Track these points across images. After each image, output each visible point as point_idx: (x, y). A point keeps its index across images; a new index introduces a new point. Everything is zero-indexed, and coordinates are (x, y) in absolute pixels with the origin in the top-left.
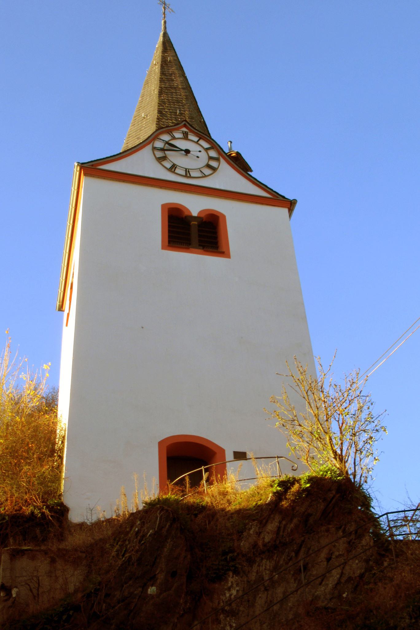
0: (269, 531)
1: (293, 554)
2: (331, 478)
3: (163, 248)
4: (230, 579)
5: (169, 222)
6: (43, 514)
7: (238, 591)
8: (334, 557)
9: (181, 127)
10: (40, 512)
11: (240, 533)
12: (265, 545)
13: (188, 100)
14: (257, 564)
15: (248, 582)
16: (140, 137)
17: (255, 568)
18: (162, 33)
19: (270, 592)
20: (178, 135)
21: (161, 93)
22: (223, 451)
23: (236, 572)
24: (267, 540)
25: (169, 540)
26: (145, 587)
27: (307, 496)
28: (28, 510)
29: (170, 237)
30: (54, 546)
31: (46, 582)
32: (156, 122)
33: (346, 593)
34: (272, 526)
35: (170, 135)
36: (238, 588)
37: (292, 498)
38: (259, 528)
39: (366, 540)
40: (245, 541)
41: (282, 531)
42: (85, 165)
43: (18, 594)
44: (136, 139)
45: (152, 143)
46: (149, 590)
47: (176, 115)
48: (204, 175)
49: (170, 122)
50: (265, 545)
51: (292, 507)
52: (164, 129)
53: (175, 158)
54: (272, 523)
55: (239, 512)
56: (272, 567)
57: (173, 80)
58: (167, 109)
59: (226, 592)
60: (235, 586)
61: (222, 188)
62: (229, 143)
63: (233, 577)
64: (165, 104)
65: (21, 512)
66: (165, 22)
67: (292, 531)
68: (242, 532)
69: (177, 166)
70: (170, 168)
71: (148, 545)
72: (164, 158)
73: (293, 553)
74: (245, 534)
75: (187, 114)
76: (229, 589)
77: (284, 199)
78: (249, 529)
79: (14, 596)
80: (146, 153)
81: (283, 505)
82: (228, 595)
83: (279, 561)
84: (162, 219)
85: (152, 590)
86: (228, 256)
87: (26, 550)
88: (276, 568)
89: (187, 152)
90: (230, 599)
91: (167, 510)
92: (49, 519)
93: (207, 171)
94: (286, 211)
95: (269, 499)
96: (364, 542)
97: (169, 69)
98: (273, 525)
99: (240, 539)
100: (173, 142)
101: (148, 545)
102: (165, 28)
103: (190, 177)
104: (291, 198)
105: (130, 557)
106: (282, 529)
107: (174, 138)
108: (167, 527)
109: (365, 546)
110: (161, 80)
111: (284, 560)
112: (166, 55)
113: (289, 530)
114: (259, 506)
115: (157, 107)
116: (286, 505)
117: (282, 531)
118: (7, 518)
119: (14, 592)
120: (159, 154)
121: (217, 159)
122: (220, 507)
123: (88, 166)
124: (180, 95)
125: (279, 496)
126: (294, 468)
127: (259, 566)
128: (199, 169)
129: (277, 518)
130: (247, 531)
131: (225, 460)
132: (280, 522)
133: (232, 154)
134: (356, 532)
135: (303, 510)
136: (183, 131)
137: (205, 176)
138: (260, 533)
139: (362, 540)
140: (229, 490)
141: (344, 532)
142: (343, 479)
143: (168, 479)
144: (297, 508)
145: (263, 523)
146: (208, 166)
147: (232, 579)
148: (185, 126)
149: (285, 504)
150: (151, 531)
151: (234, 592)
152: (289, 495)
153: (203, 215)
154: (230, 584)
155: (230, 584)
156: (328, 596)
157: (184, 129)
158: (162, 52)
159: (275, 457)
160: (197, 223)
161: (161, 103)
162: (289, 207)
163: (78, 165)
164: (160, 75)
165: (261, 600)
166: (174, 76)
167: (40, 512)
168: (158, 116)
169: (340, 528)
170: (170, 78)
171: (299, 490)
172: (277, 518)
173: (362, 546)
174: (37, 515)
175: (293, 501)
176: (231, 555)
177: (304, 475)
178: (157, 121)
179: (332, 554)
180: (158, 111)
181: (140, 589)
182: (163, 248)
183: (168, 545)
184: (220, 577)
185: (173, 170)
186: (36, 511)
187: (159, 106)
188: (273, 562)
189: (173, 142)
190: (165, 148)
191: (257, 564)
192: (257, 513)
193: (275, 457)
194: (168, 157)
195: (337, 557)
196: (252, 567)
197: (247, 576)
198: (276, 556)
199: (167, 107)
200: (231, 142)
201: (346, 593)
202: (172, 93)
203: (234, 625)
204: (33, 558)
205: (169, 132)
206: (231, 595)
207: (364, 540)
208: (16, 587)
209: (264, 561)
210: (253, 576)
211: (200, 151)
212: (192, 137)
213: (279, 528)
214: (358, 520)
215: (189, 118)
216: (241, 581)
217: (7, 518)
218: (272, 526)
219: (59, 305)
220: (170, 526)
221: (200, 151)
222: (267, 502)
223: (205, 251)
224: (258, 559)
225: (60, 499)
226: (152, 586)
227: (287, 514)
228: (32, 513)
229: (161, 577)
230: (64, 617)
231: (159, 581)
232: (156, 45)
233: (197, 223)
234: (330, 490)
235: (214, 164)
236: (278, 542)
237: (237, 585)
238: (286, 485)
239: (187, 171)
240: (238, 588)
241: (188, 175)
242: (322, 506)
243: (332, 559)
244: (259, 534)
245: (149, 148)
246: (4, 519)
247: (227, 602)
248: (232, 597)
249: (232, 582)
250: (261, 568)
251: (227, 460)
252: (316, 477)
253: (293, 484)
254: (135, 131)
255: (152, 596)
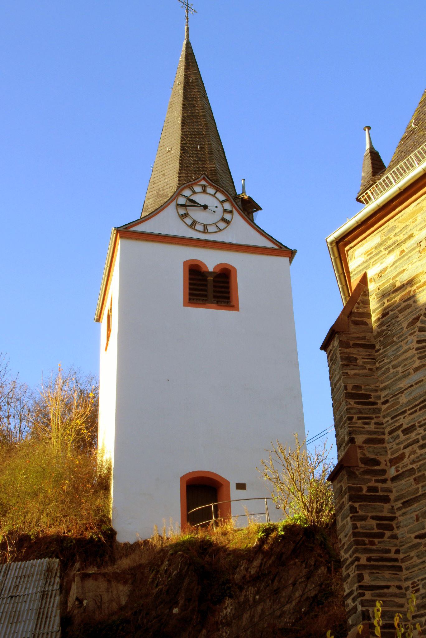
0: (254, 566)
1: (270, 582)
2: (300, 525)
3: (185, 305)
4: (227, 602)
5: (190, 274)
6: (99, 538)
7: (231, 609)
8: (298, 583)
9: (200, 181)
10: (97, 537)
11: (235, 568)
12: (251, 576)
13: (207, 130)
14: (245, 590)
15: (239, 603)
16: (165, 174)
17: (243, 593)
18: (185, 42)
19: (253, 610)
20: (198, 189)
21: (183, 124)
22: (228, 483)
23: (231, 597)
24: (252, 573)
25: (187, 578)
26: (171, 609)
27: (281, 540)
28: (88, 534)
29: (190, 294)
30: (110, 569)
31: (105, 598)
32: (178, 178)
33: (304, 608)
34: (256, 563)
35: (191, 189)
36: (232, 607)
37: (272, 543)
38: (248, 565)
39: (321, 569)
40: (238, 574)
41: (263, 566)
42: (120, 229)
43: (88, 604)
44: (162, 176)
45: (175, 201)
46: (174, 610)
47: (197, 150)
48: (219, 230)
49: (192, 160)
50: (251, 576)
51: (271, 549)
52: (186, 185)
53: (196, 214)
54: (256, 560)
55: (235, 551)
56: (255, 592)
57: (194, 106)
58: (189, 144)
59: (224, 610)
60: (230, 606)
61: (235, 242)
62: (243, 180)
63: (229, 600)
64: (187, 138)
65: (84, 536)
66: (188, 29)
67: (270, 565)
68: (236, 569)
69: (197, 222)
70: (191, 225)
71: (173, 582)
72: (186, 215)
73: (270, 581)
74: (238, 569)
75: (206, 148)
76: (226, 608)
77: (289, 250)
78: (241, 566)
79: (85, 605)
80: (171, 211)
81: (264, 548)
82: (225, 612)
83: (260, 587)
84: (181, 518)
85: (176, 610)
86: (238, 310)
87: (92, 574)
88: (257, 593)
89: (205, 207)
90: (226, 615)
91: (186, 557)
92: (103, 542)
93: (222, 225)
94: (287, 259)
95: (255, 543)
96: (320, 572)
97: (191, 92)
98: (257, 562)
99: (234, 574)
100: (193, 198)
101: (173, 582)
102: (188, 36)
103: (208, 232)
104: (292, 248)
105: (162, 589)
106: (263, 564)
107: (194, 193)
108: (186, 569)
109: (320, 574)
110: (184, 107)
111: (264, 586)
112: (189, 73)
113: (268, 565)
114: (248, 548)
115: (179, 142)
116: (266, 548)
117: (263, 566)
118: (74, 541)
119: (85, 602)
120: (182, 211)
121: (230, 212)
122: (222, 544)
123: (122, 230)
124: (201, 125)
125: (262, 541)
126: (277, 507)
127: (246, 591)
128: (215, 223)
129: (261, 556)
130: (239, 567)
131: (230, 499)
132: (262, 560)
133: (244, 197)
134: (315, 564)
135: (278, 550)
136: (202, 185)
137: (220, 230)
138: (248, 568)
139: (318, 570)
140: (229, 530)
141: (306, 564)
142: (308, 526)
143: (188, 522)
144: (275, 549)
145: (250, 561)
146: (223, 220)
147: (228, 601)
148: (204, 179)
149: (266, 547)
150: (175, 572)
151: (229, 610)
152: (270, 541)
153: (217, 271)
154: (226, 605)
155: (226, 605)
156: (292, 611)
157: (203, 182)
158: (185, 69)
159: (264, 498)
160: (212, 278)
161: (184, 137)
162: (290, 256)
163: (115, 230)
164: (183, 101)
165: (246, 616)
166: (196, 101)
167: (97, 537)
168: (181, 153)
169: (304, 561)
170: (192, 104)
171: (276, 536)
172: (261, 556)
173: (318, 575)
174: (95, 539)
175: (272, 545)
176: (228, 585)
177: (282, 523)
178: (181, 134)
179: (296, 581)
180: (181, 147)
181: (168, 610)
182: (185, 305)
183: (186, 581)
184: (220, 601)
185: (193, 227)
186: (94, 537)
187: (182, 141)
188: (256, 589)
189: (194, 198)
190: (187, 204)
191: (245, 590)
192: (246, 554)
193: (264, 498)
194: (189, 214)
195: (300, 583)
196: (241, 592)
197: (238, 599)
198: (258, 583)
199: (189, 141)
200: (244, 180)
201: (304, 608)
202: (193, 122)
203: (228, 632)
204: (96, 579)
205: (190, 187)
206: (227, 612)
207: (320, 570)
208: (86, 599)
209: (250, 588)
210: (242, 599)
211: (216, 207)
212: (211, 191)
213: (261, 564)
214: (316, 555)
215: (208, 153)
216: (234, 602)
217: (74, 541)
218: (256, 563)
219: (97, 318)
220: (188, 568)
221: (216, 207)
222: (254, 546)
223: (219, 305)
224: (246, 587)
225: (110, 525)
226: (176, 607)
227: (267, 554)
228: (92, 537)
229: (181, 602)
230: (121, 628)
231: (180, 605)
232: (179, 58)
233: (212, 278)
234: (298, 534)
235: (228, 216)
236: (260, 574)
237: (231, 605)
238: (268, 531)
239: (205, 226)
240: (232, 607)
241: (206, 231)
242: (292, 547)
243: (297, 585)
244: (247, 569)
245: (173, 205)
246: (72, 542)
247: (224, 617)
248: (228, 613)
249: (228, 604)
250: (248, 593)
251: (232, 499)
252: (289, 525)
253: (272, 531)
254: (160, 164)
255: (176, 614)
